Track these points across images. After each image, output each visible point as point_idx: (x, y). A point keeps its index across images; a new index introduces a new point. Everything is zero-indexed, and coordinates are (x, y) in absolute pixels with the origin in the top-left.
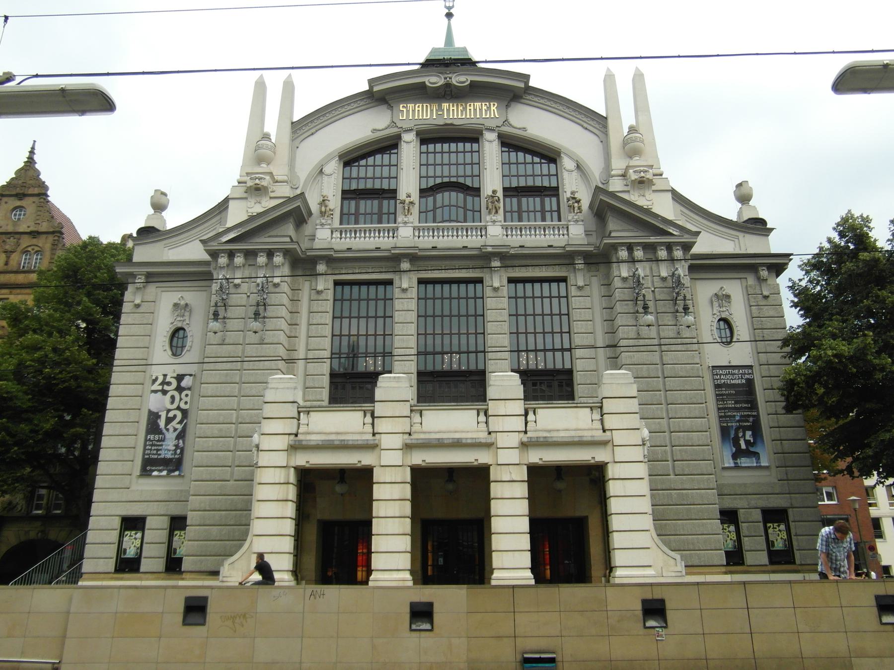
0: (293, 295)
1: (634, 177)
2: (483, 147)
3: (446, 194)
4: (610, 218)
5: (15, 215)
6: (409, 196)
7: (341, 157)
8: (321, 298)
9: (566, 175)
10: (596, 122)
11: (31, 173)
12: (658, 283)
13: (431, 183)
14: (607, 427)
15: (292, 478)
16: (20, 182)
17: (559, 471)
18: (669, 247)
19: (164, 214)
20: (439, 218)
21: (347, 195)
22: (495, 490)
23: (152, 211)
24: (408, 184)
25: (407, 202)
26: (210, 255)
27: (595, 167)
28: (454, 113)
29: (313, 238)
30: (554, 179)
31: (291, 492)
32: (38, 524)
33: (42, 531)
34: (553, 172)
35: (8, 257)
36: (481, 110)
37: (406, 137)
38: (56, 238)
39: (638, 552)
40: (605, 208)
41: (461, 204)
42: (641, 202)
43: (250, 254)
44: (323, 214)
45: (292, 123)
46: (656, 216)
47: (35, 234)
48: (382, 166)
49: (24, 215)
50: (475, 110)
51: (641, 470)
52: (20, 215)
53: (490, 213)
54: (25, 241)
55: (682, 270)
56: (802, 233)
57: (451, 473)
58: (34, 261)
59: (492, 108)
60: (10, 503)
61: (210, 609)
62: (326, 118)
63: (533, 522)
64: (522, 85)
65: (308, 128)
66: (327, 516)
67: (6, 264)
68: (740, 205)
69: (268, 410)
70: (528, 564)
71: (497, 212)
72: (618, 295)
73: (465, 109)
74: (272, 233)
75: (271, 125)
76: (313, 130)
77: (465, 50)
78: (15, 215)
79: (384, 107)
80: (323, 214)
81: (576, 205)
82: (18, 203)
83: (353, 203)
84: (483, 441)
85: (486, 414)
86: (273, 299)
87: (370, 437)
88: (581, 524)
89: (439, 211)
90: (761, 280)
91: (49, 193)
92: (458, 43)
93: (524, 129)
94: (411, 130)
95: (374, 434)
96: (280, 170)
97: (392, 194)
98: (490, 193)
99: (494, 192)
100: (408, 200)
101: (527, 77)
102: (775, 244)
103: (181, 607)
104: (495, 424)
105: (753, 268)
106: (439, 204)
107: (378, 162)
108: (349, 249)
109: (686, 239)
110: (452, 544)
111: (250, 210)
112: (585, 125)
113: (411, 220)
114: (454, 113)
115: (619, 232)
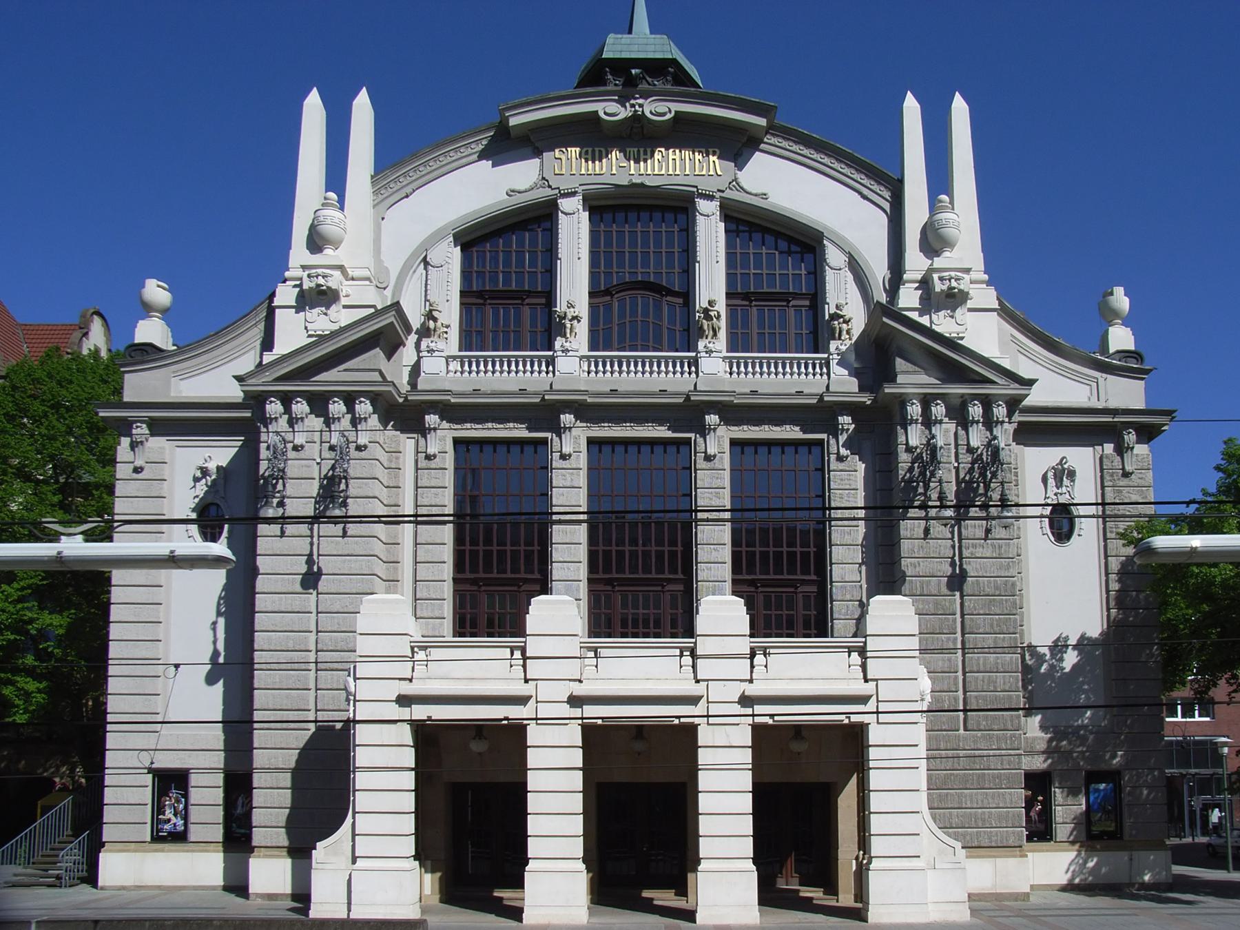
6: (570, 306)
8: (433, 466)
9: (830, 275)
14: (869, 677)
27: (879, 270)
37: (565, 204)
43: (319, 403)
51: (918, 734)
55: (1004, 434)
63: (759, 791)
70: (750, 852)
71: (715, 334)
81: (844, 326)
85: (693, 654)
86: (355, 468)
90: (1121, 450)
93: (764, 196)
98: (705, 305)
109: (1014, 390)
110: (641, 828)
111: (310, 326)
113: (575, 347)
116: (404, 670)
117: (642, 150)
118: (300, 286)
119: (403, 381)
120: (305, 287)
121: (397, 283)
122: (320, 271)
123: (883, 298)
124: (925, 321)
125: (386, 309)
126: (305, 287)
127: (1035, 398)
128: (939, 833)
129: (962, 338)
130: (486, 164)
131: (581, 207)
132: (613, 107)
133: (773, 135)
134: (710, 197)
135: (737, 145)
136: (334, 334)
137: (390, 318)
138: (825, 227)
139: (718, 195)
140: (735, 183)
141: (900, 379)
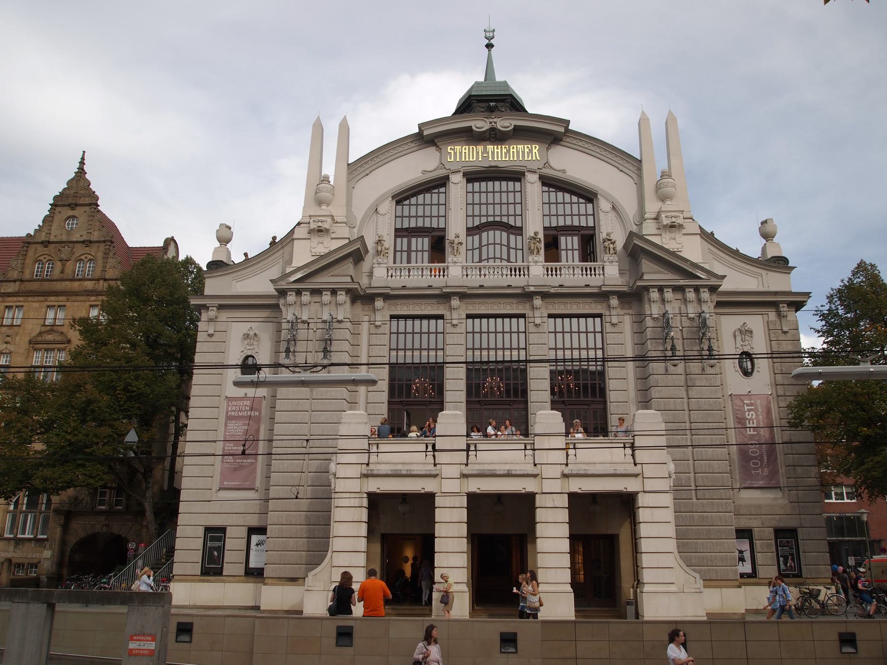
0: (354, 329)
1: (666, 222)
3: (491, 233)
4: (643, 260)
5: (68, 224)
7: (393, 197)
10: (633, 165)
11: (82, 183)
12: (686, 323)
14: (637, 462)
15: (365, 502)
16: (72, 192)
17: (594, 497)
18: (697, 289)
19: (229, 246)
21: (399, 233)
22: (540, 515)
23: (218, 244)
25: (456, 242)
27: (630, 209)
28: (499, 155)
29: (371, 275)
31: (364, 515)
32: (103, 518)
33: (107, 525)
34: (590, 211)
35: (64, 266)
36: (523, 152)
37: (457, 179)
38: (107, 247)
39: (669, 588)
40: (636, 252)
41: (505, 242)
42: (670, 245)
44: (378, 253)
45: (348, 165)
46: (685, 260)
47: (87, 243)
48: (431, 205)
49: (77, 224)
50: (518, 152)
51: (667, 500)
52: (73, 224)
53: (532, 253)
54: (79, 250)
55: (708, 308)
56: (819, 277)
57: (499, 498)
58: (88, 269)
59: (534, 151)
60: (76, 498)
61: (355, 635)
62: (379, 160)
64: (562, 130)
65: (363, 169)
66: (389, 530)
67: (62, 272)
68: (764, 241)
69: (342, 444)
72: (649, 333)
73: (508, 151)
74: (335, 273)
75: (329, 169)
76: (368, 172)
77: (505, 84)
78: (68, 224)
80: (378, 253)
81: (611, 246)
82: (71, 213)
83: (405, 240)
84: (530, 473)
85: (633, 447)
86: (336, 334)
87: (432, 467)
88: (612, 541)
89: (484, 249)
90: (779, 315)
91: (99, 202)
92: (499, 78)
93: (564, 171)
95: (435, 465)
96: (339, 212)
98: (533, 235)
99: (536, 233)
100: (457, 241)
101: (568, 122)
102: (795, 283)
103: (334, 634)
104: (541, 457)
105: (774, 305)
106: (484, 242)
107: (428, 201)
108: (404, 287)
109: (713, 282)
111: (313, 250)
112: (621, 167)
113: (460, 260)
114: (499, 155)
115: (652, 274)
116: (364, 458)
120: (312, 227)
121: (360, 224)
122: (320, 218)
123: (635, 229)
124: (656, 240)
125: (355, 241)
127: (726, 286)
128: (687, 569)
137: (358, 245)
140: (547, 164)
141: (646, 277)
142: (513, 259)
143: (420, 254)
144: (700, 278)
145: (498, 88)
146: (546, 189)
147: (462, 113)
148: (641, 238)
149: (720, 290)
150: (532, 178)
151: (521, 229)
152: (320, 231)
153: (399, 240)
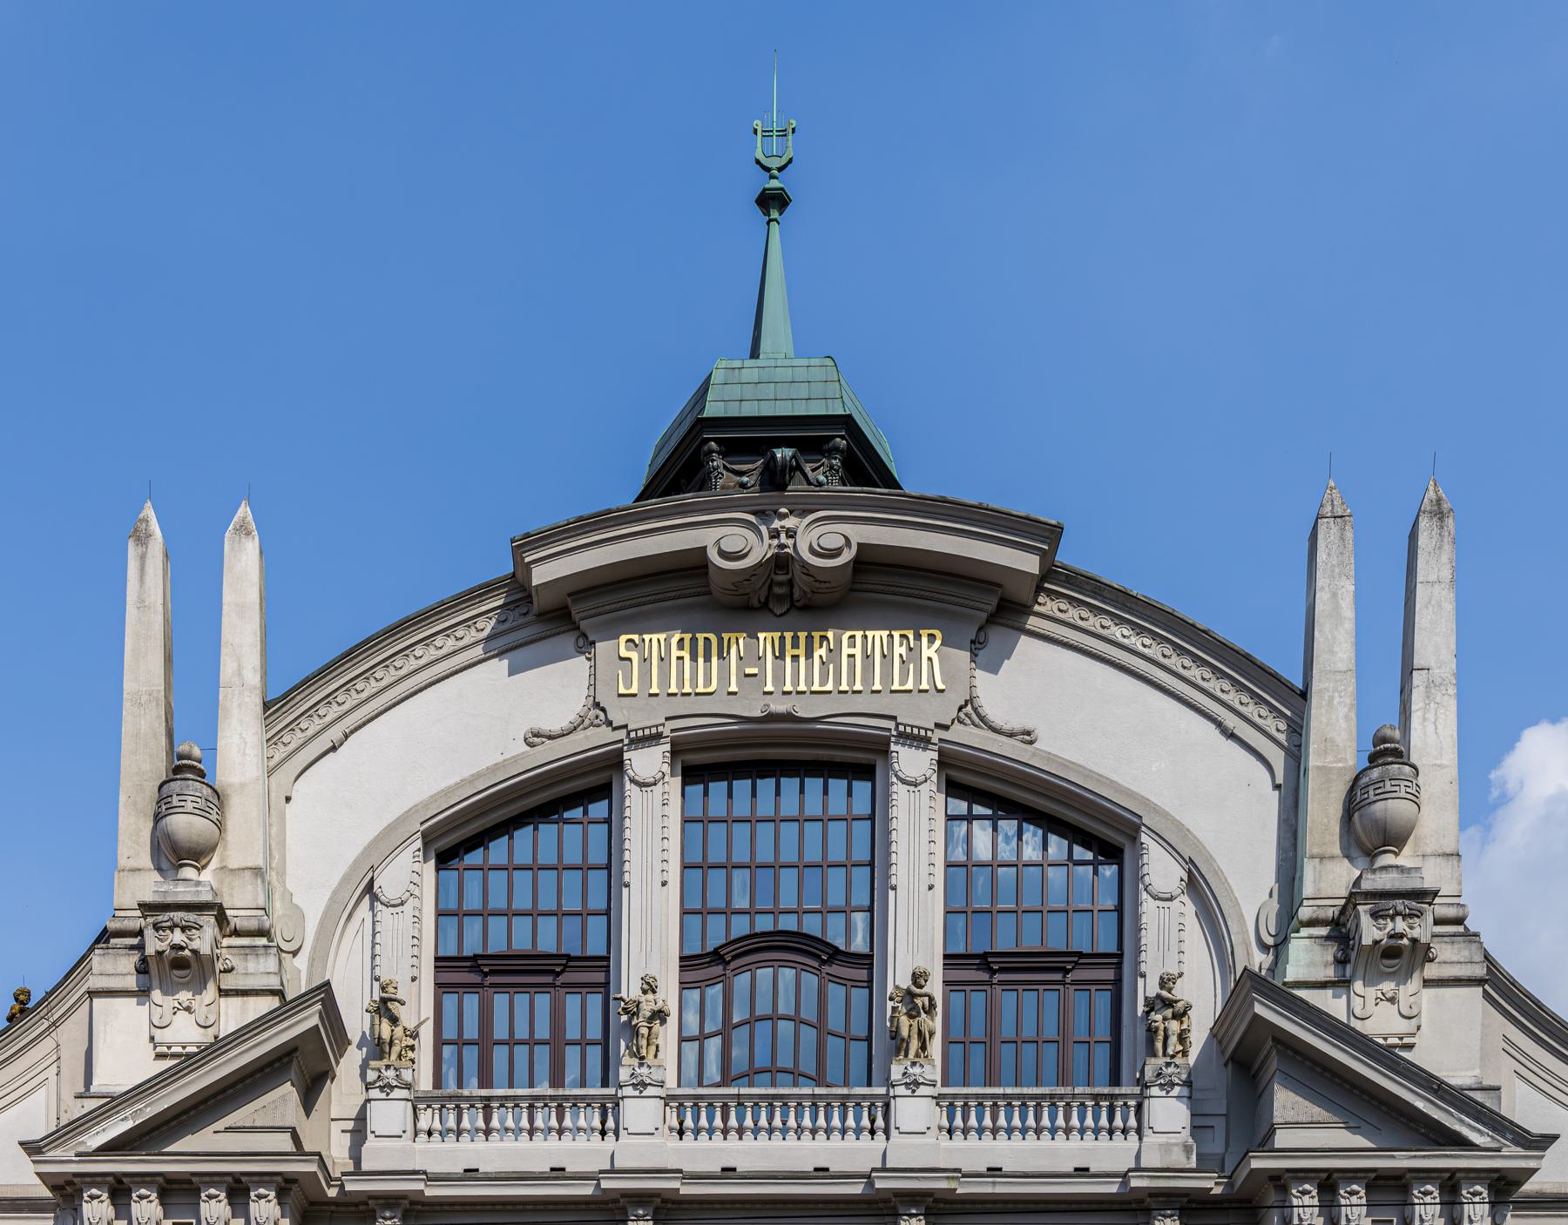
2: (622, 808)
3: (764, 974)
7: (428, 838)
9: (1149, 909)
13: (716, 939)
18: (1450, 1184)
20: (1007, 1068)
21: (461, 971)
24: (650, 941)
26: (53, 1188)
27: (1250, 892)
30: (596, 925)
37: (647, 762)
42: (1381, 1023)
64: (1029, 564)
73: (834, 653)
79: (568, 641)
81: (1174, 1026)
83: (471, 1002)
89: (739, 1036)
93: (1027, 737)
94: (655, 738)
97: (597, 970)
98: (905, 982)
99: (918, 978)
101: (1053, 534)
109: (1511, 1158)
111: (158, 1034)
112: (1231, 721)
113: (656, 1075)
115: (1303, 1128)
117: (788, 635)
118: (140, 947)
119: (338, 1151)
120: (150, 950)
121: (317, 939)
123: (1259, 960)
124: (1332, 1004)
125: (303, 1000)
126: (150, 950)
129: (1410, 1047)
130: (500, 666)
131: (666, 768)
132: (735, 537)
133: (1050, 593)
134: (918, 740)
135: (987, 611)
136: (218, 1046)
138: (1146, 802)
139: (936, 735)
140: (970, 711)
141: (1282, 1139)
142: (834, 1067)
143: (521, 1052)
144: (1462, 1143)
145: (803, 391)
146: (960, 807)
147: (674, 488)
148: (1283, 997)
149: (1530, 1186)
150: (913, 762)
151: (864, 960)
152: (180, 964)
153: (450, 1001)
